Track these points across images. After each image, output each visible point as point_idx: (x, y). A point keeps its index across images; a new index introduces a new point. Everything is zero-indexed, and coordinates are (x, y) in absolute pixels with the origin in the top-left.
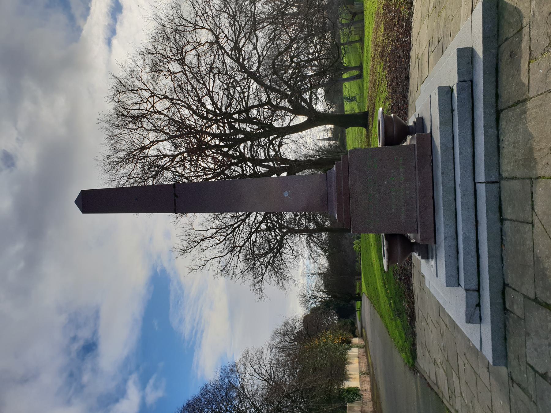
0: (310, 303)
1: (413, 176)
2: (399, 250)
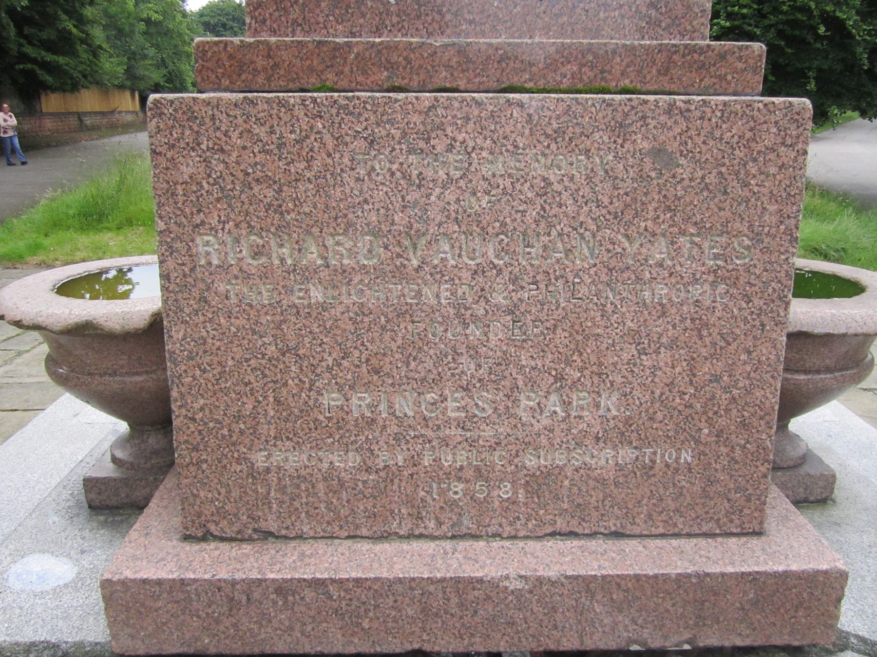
1: (561, 524)
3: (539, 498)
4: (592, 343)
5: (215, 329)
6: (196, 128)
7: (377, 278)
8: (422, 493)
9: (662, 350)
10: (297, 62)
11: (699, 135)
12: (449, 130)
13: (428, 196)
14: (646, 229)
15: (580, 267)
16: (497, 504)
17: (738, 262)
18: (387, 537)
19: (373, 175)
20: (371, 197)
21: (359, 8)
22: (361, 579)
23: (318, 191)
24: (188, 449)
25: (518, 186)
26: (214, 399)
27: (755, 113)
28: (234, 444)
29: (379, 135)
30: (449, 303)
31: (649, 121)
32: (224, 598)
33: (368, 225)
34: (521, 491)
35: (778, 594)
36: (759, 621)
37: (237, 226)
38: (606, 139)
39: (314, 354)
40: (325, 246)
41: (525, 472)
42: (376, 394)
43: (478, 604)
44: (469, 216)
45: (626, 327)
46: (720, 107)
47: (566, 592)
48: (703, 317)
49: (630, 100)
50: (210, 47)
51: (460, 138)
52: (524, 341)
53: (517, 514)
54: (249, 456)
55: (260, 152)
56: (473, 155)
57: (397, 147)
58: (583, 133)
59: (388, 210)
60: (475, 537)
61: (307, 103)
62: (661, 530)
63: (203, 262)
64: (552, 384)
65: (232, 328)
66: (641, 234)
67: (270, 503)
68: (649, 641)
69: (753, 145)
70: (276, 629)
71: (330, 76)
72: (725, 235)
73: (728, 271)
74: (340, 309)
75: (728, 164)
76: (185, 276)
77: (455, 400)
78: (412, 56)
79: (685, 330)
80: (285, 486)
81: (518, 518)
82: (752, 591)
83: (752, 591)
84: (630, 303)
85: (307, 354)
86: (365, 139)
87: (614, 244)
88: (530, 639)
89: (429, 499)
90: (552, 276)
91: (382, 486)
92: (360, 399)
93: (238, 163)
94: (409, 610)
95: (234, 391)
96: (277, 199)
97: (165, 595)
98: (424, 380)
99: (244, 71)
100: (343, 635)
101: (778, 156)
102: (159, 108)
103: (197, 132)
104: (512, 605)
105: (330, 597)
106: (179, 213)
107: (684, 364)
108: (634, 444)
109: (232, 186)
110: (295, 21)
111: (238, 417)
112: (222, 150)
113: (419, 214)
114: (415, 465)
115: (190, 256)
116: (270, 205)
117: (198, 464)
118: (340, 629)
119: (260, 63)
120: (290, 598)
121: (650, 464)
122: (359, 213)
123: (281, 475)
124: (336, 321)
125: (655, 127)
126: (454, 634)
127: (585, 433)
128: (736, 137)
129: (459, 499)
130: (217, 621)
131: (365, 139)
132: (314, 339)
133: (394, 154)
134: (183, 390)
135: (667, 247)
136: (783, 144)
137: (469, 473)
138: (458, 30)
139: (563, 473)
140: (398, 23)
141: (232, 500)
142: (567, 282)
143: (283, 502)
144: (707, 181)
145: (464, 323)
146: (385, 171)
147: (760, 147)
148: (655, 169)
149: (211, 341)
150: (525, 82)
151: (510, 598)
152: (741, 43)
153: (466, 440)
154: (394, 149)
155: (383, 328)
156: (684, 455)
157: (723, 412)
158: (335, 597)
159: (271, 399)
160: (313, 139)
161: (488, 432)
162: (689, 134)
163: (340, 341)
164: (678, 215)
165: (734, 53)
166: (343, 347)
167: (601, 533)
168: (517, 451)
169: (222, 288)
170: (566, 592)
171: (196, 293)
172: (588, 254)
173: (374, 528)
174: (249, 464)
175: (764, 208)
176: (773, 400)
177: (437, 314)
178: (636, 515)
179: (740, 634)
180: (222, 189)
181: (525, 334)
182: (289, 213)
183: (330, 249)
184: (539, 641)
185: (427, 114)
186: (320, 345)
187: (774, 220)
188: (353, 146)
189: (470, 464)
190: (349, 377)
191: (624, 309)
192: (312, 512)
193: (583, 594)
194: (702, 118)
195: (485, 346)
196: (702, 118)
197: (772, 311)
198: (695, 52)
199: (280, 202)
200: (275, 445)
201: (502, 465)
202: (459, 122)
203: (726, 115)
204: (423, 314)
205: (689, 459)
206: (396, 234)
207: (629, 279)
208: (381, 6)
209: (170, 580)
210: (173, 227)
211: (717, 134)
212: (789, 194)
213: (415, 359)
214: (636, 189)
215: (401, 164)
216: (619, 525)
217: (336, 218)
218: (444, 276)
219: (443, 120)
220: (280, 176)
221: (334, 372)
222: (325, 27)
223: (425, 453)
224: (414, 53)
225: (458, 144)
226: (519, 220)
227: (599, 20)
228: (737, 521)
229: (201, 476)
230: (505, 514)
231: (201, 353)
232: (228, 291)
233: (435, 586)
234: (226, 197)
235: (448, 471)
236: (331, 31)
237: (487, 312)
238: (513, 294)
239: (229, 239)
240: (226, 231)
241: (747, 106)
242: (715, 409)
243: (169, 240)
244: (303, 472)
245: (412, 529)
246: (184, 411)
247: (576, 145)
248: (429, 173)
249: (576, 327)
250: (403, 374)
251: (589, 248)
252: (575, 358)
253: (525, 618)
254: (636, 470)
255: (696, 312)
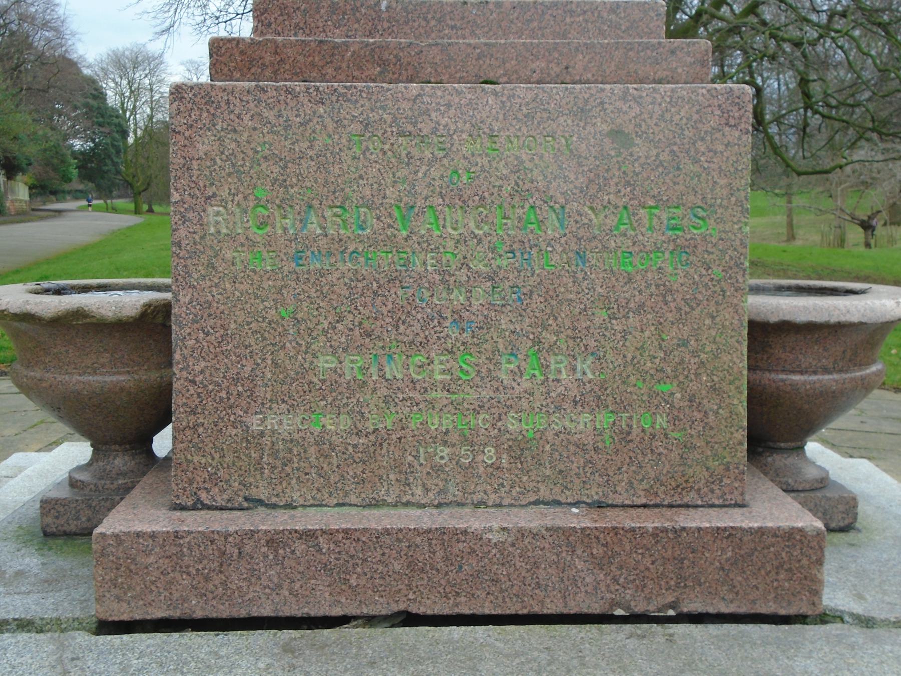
0: (118, 80)
1: (544, 492)
2: (111, 376)
3: (521, 463)
4: (565, 308)
5: (221, 294)
6: (212, 111)
7: (370, 246)
8: (410, 458)
9: (631, 314)
10: (301, 58)
11: (651, 118)
12: (433, 115)
13: (416, 172)
14: (609, 203)
15: (552, 237)
16: (482, 469)
17: (695, 231)
18: (375, 505)
19: (368, 154)
20: (366, 173)
21: (354, 15)
22: (350, 529)
23: (319, 168)
24: (186, 412)
25: (494, 164)
26: (215, 361)
27: (700, 98)
28: (231, 407)
29: (373, 119)
30: (435, 270)
31: (606, 106)
32: (216, 553)
33: (362, 198)
34: (504, 456)
35: (756, 553)
36: (740, 583)
37: (245, 198)
38: (569, 122)
39: (311, 317)
40: (323, 217)
41: (508, 436)
42: (368, 356)
43: (462, 557)
44: (452, 191)
45: (596, 293)
46: (669, 94)
47: (547, 546)
48: (667, 283)
49: (589, 88)
50: (224, 44)
51: (443, 122)
52: (503, 306)
53: (501, 481)
54: (244, 419)
55: (268, 133)
56: (455, 137)
57: (389, 130)
58: (549, 117)
59: (380, 185)
60: (461, 505)
61: (311, 91)
62: (644, 501)
63: (212, 230)
64: (530, 348)
65: (236, 292)
66: (605, 207)
67: (262, 468)
68: (633, 603)
69: (700, 126)
70: (265, 588)
71: (329, 71)
72: (681, 207)
73: (686, 240)
74: (336, 275)
75: (679, 142)
76: (195, 243)
77: (441, 363)
78: (401, 54)
79: (651, 295)
80: (278, 451)
81: (502, 485)
82: (730, 549)
83: (730, 549)
84: (598, 270)
85: (305, 318)
86: (361, 122)
87: (581, 216)
88: (515, 599)
89: (416, 464)
90: (527, 245)
91: (372, 449)
92: (352, 362)
93: (248, 142)
94: (396, 564)
95: (235, 354)
96: (282, 175)
97: (157, 550)
98: (412, 343)
99: (254, 66)
100: (331, 594)
101: (723, 135)
102: (180, 93)
103: (213, 114)
104: (495, 560)
105: (320, 550)
106: (193, 185)
107: (653, 328)
108: (611, 408)
109: (242, 163)
110: (297, 25)
111: (236, 380)
112: (235, 131)
113: (408, 188)
114: (404, 429)
115: (201, 225)
116: (276, 180)
117: (194, 428)
118: (329, 586)
119: (268, 58)
120: (281, 551)
121: (627, 429)
122: (355, 187)
123: (274, 439)
124: (332, 286)
125: (612, 112)
126: (439, 592)
127: (563, 397)
128: (684, 119)
129: (445, 464)
130: (207, 579)
131: (361, 122)
132: (312, 303)
133: (385, 135)
134: (186, 352)
135: (629, 219)
136: (727, 124)
137: (454, 438)
138: (441, 34)
139: (544, 438)
140: (389, 28)
141: (225, 466)
142: (541, 250)
143: (275, 467)
144: (661, 158)
145: (448, 289)
146: (378, 151)
147: (707, 127)
148: (615, 148)
149: (215, 305)
150: (500, 77)
151: (494, 551)
152: (688, 40)
153: (452, 403)
154: (386, 132)
155: (375, 293)
156: (659, 419)
157: (693, 376)
158: (324, 550)
159: (269, 362)
160: (315, 121)
161: (472, 395)
162: (643, 117)
163: (335, 305)
164: (637, 189)
165: (683, 48)
166: (338, 311)
167: (584, 503)
168: (500, 414)
169: (229, 255)
170: (547, 546)
171: (204, 259)
172: (558, 225)
173: (363, 495)
174: (244, 428)
175: (715, 182)
176: (741, 365)
177: (424, 280)
178: (617, 483)
179: (723, 598)
180: (233, 165)
181: (504, 299)
182: (292, 187)
183: (329, 220)
184: (523, 601)
185: (414, 101)
186: (317, 309)
187: (725, 192)
188: (350, 129)
189: (455, 427)
190: (343, 340)
191: (593, 276)
192: (304, 478)
193: (564, 548)
194: (653, 103)
195: (468, 311)
196: (653, 103)
197: (730, 278)
198: (648, 48)
199: (285, 177)
200: (270, 409)
201: (486, 429)
202: (442, 108)
203: (674, 100)
204: (411, 280)
205: (665, 425)
206: (387, 206)
207: (597, 248)
208: (374, 13)
209: (164, 532)
210: (187, 198)
211: (668, 116)
212: (737, 169)
213: (404, 323)
214: (598, 166)
215: (392, 144)
216: (601, 494)
217: (334, 192)
218: (430, 244)
219: (429, 107)
220: (286, 154)
221: (329, 335)
222: (324, 31)
223: (412, 415)
224: (403, 51)
225: (441, 127)
226: (496, 194)
227: (566, 25)
228: (717, 491)
229: (196, 440)
230: (489, 481)
231: (205, 315)
232: (234, 258)
233: (422, 537)
234: (237, 172)
235: (434, 435)
236: (329, 34)
237: (469, 278)
238: (492, 261)
239: (238, 210)
240: (236, 203)
241: (693, 92)
242: (686, 373)
243: (182, 210)
244: (296, 436)
245: (399, 496)
246: (185, 374)
247: (544, 128)
248: (415, 152)
249: (551, 293)
250: (393, 336)
251: (558, 219)
252: (550, 322)
253: (508, 575)
254: (613, 435)
255: (660, 279)
